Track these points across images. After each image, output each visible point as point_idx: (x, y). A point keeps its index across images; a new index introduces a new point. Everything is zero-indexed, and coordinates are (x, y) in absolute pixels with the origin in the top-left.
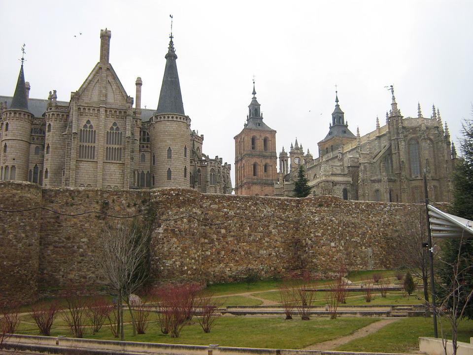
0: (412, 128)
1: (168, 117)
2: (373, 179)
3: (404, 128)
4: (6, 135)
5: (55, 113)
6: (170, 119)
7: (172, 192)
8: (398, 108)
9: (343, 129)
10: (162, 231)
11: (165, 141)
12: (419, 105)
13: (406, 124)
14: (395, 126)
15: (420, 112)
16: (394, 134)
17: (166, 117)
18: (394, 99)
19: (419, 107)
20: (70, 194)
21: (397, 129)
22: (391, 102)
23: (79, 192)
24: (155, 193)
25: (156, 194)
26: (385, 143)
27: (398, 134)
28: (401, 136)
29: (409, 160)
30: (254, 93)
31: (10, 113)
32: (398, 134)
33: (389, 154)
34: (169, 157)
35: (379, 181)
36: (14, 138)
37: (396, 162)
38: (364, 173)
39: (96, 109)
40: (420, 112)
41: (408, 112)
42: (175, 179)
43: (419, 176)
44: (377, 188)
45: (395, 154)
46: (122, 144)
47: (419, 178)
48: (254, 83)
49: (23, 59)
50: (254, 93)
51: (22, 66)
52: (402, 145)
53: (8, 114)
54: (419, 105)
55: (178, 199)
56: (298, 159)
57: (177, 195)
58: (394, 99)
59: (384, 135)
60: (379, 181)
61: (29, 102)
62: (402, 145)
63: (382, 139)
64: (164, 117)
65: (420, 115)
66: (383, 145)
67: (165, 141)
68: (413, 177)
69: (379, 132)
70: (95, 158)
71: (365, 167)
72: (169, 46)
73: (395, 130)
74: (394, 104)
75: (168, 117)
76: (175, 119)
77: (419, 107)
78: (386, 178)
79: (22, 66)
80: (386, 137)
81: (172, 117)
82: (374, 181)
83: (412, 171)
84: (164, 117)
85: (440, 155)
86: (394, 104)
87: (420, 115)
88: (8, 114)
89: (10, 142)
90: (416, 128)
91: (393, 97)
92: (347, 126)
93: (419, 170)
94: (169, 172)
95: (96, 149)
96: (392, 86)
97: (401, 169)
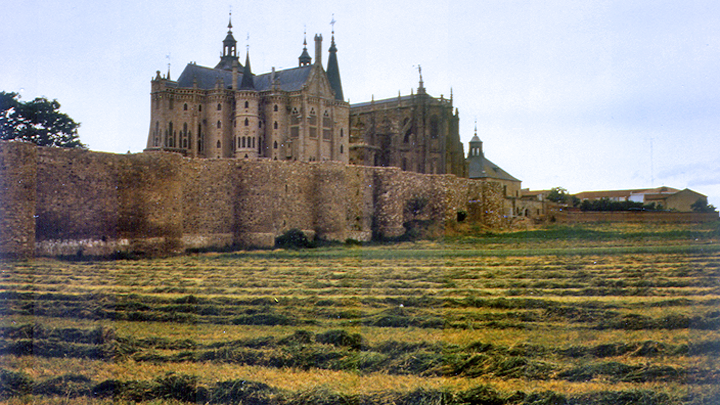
8: (424, 86)
18: (421, 77)
22: (419, 80)
30: (230, 26)
58: (421, 77)
61: (255, 80)
86: (421, 83)
94: (342, 147)
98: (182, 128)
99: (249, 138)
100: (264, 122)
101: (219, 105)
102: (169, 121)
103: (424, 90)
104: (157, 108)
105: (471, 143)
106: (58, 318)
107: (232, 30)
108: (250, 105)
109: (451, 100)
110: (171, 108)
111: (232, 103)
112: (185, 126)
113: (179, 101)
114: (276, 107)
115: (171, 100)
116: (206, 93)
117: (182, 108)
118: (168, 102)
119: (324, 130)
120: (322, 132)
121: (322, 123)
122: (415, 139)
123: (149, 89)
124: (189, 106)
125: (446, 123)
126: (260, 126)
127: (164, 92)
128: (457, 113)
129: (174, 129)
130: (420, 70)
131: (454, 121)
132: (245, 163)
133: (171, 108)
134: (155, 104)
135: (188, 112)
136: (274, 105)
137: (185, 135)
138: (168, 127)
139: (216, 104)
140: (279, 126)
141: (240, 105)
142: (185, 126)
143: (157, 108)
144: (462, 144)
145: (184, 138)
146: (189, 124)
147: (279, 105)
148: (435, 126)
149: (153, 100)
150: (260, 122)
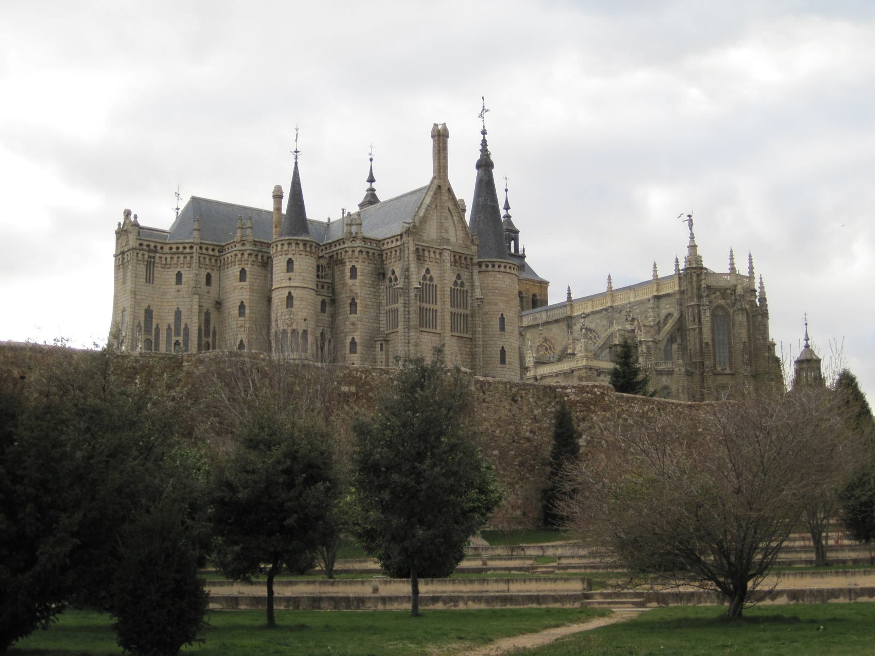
0: (719, 290)
1: (499, 266)
2: (659, 368)
3: (709, 287)
4: (290, 279)
5: (363, 249)
6: (502, 269)
7: (596, 390)
8: (699, 253)
9: (516, 262)
10: (585, 444)
11: (496, 304)
12: (731, 251)
13: (713, 283)
14: (695, 285)
15: (732, 264)
16: (692, 297)
17: (497, 266)
18: (692, 237)
19: (732, 255)
20: (481, 387)
21: (699, 288)
22: (687, 242)
23: (489, 384)
24: (567, 388)
25: (569, 391)
26: (668, 308)
27: (700, 297)
28: (705, 301)
29: (713, 340)
30: (371, 180)
31: (283, 245)
32: (700, 297)
33: (680, 328)
34: (502, 328)
35: (670, 373)
36: (305, 285)
37: (695, 344)
38: (647, 357)
39: (438, 251)
40: (732, 264)
41: (715, 263)
42: (510, 364)
43: (728, 368)
44: (665, 383)
45: (694, 329)
46: (469, 308)
47: (728, 371)
48: (371, 160)
49: (296, 152)
50: (371, 180)
51: (296, 163)
52: (706, 317)
53: (279, 246)
54: (731, 251)
55: (603, 398)
56: (197, 297)
57: (603, 393)
58: (692, 237)
59: (668, 295)
60: (670, 373)
61: (310, 226)
62: (706, 317)
63: (663, 301)
64: (493, 266)
65: (733, 269)
66: (664, 312)
67: (496, 304)
68: (719, 369)
69: (658, 290)
70: (439, 328)
71: (648, 348)
72: (481, 147)
73: (695, 291)
74: (693, 247)
75: (499, 266)
76: (508, 270)
77: (732, 255)
78: (683, 370)
79: (296, 163)
80: (673, 300)
81: (505, 267)
82: (660, 373)
83: (717, 359)
84: (493, 266)
85: (758, 336)
86: (693, 247)
87: (733, 269)
88: (279, 246)
89: (298, 291)
90: (726, 289)
91: (692, 234)
92: (523, 257)
93: (727, 360)
94: (503, 352)
95: (438, 314)
96: (689, 216)
97: (702, 354)
98: (171, 319)
99: (294, 331)
100: (333, 301)
101: (243, 272)
102: (145, 305)
103: (698, 260)
104: (124, 282)
105: (799, 362)
106: (402, 595)
107: (374, 185)
108: (296, 266)
109: (751, 277)
110: (149, 279)
111: (266, 264)
112: (178, 314)
113: (165, 266)
114: (353, 270)
115: (150, 265)
116: (222, 249)
117: (173, 280)
118: (142, 268)
119: (453, 314)
120: (448, 317)
121: (448, 300)
122: (683, 349)
123: (109, 247)
124: (187, 276)
125: (741, 318)
126: (323, 310)
127: (140, 250)
128: (763, 300)
129: (155, 322)
130: (691, 225)
131: (758, 315)
132: (201, 361)
133: (149, 279)
134: (121, 274)
135: (183, 287)
136: (348, 266)
137: (177, 334)
138: (142, 319)
139: (235, 270)
140: (248, 276)
141: (279, 264)
142: (178, 314)
143: (124, 282)
144: (777, 360)
145: (174, 339)
146: (184, 312)
147: (358, 267)
148: (722, 317)
149: (117, 268)
150: (323, 303)
